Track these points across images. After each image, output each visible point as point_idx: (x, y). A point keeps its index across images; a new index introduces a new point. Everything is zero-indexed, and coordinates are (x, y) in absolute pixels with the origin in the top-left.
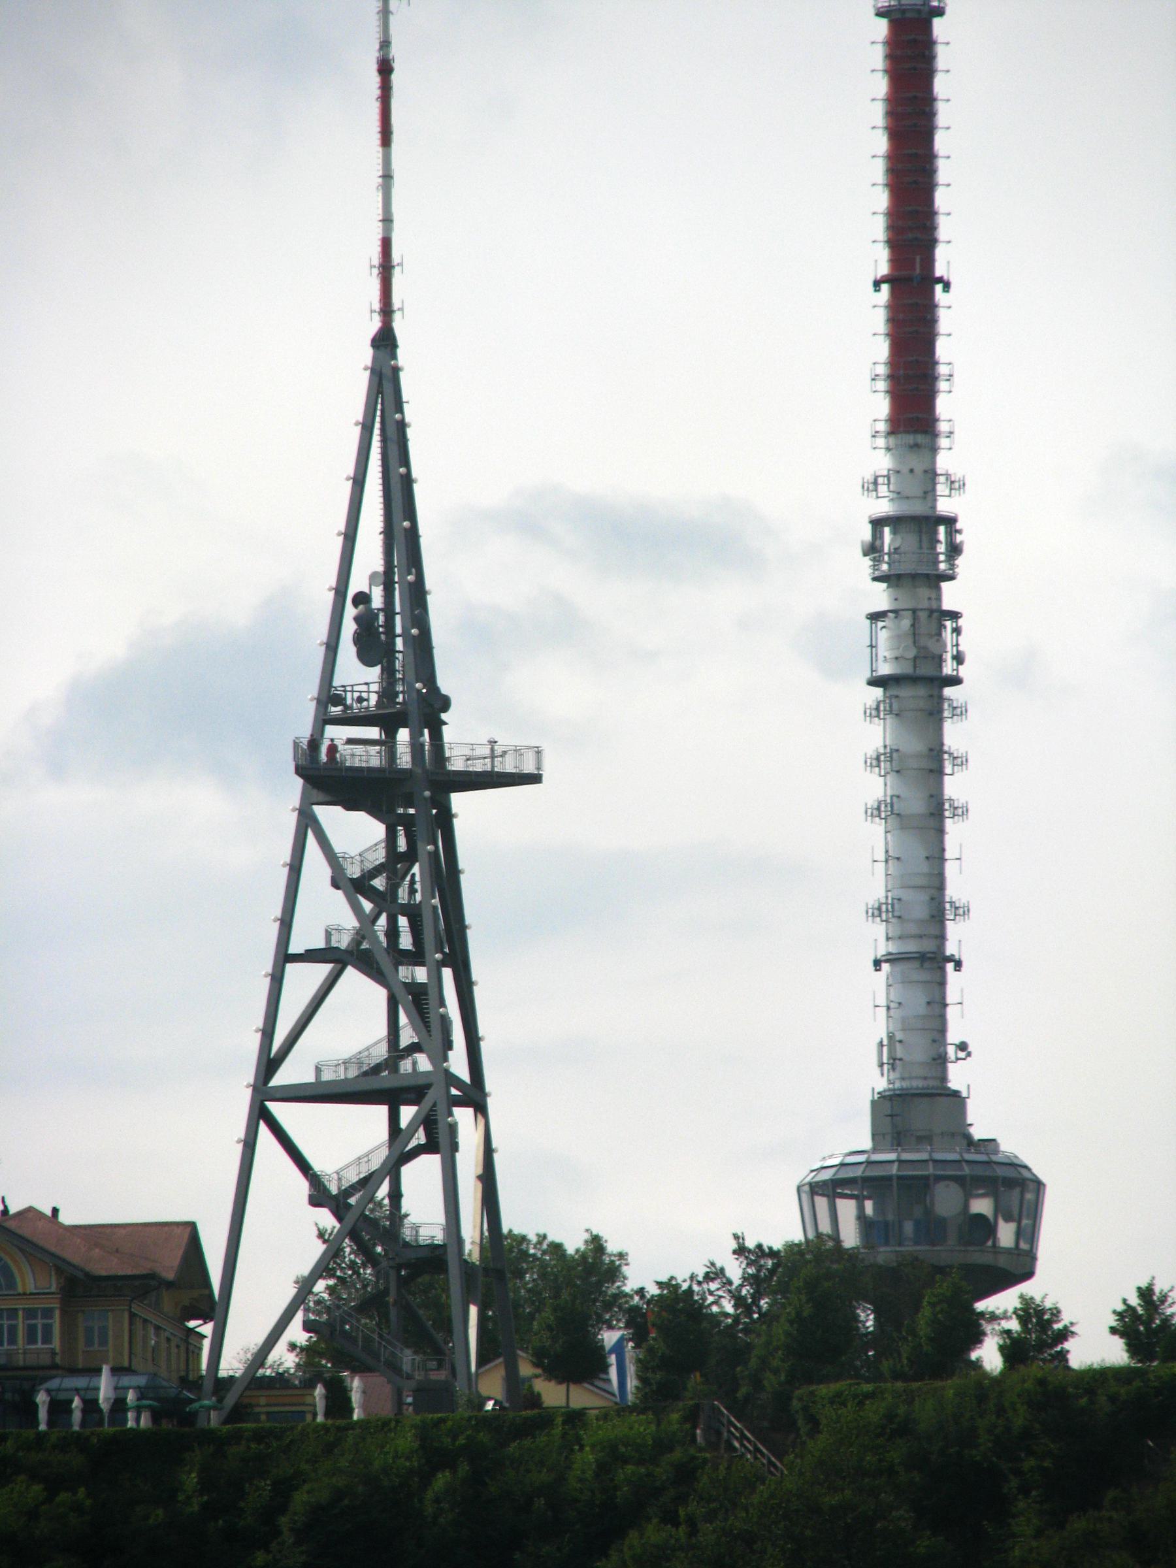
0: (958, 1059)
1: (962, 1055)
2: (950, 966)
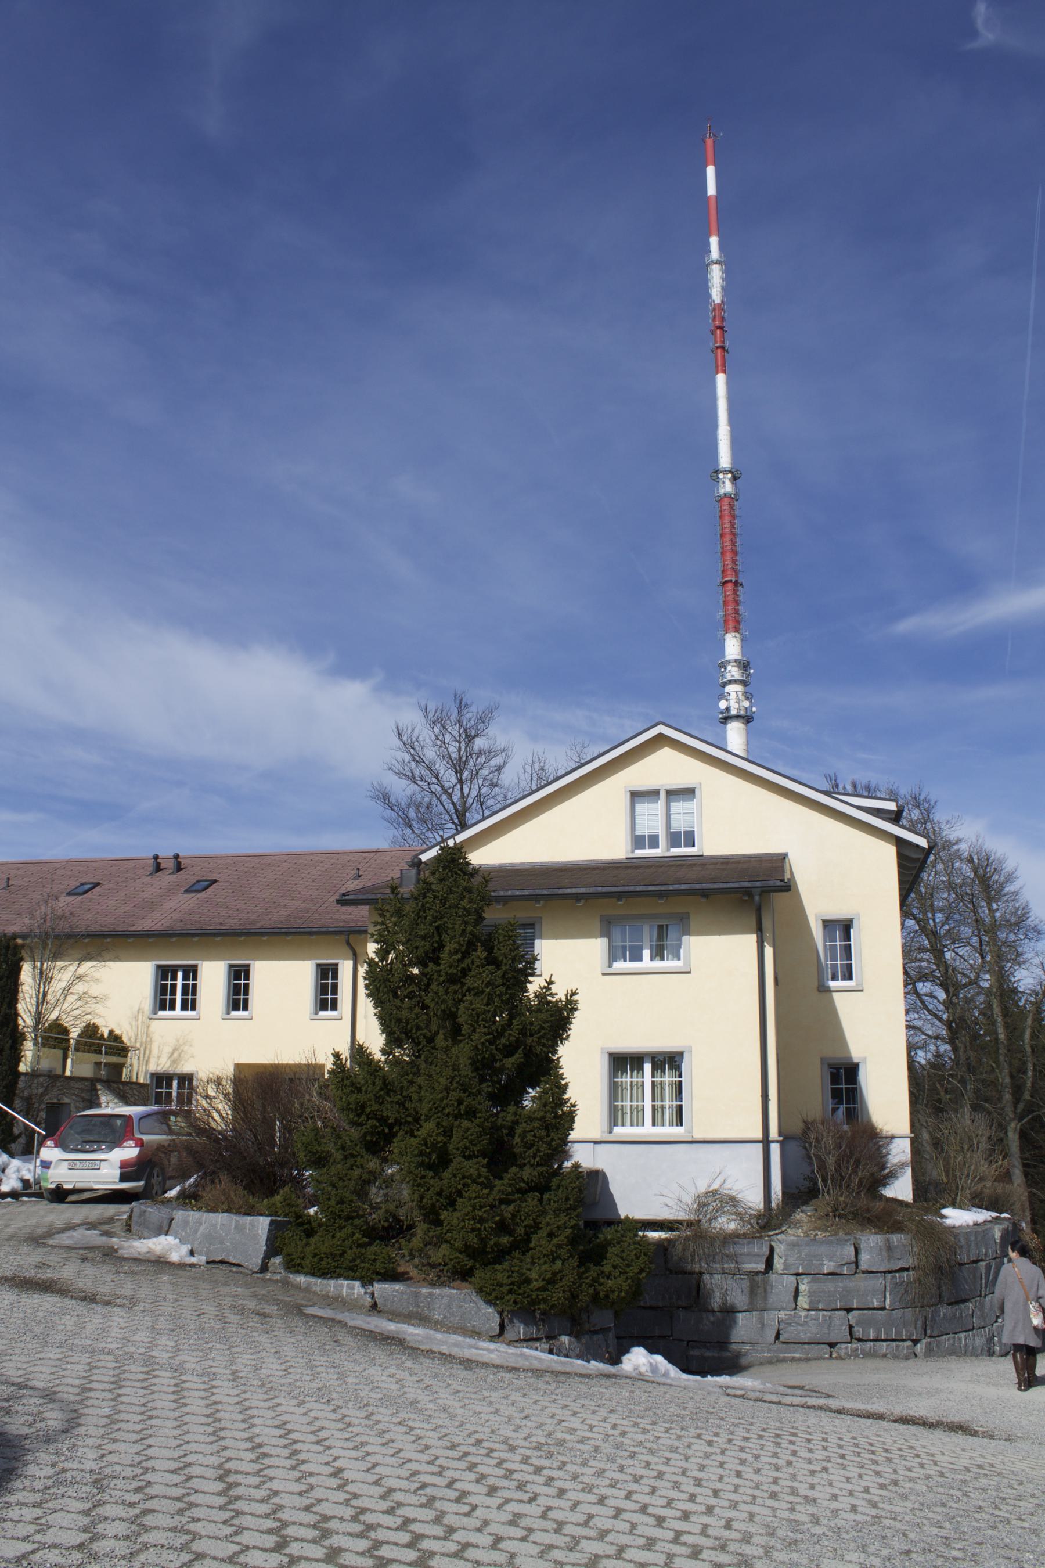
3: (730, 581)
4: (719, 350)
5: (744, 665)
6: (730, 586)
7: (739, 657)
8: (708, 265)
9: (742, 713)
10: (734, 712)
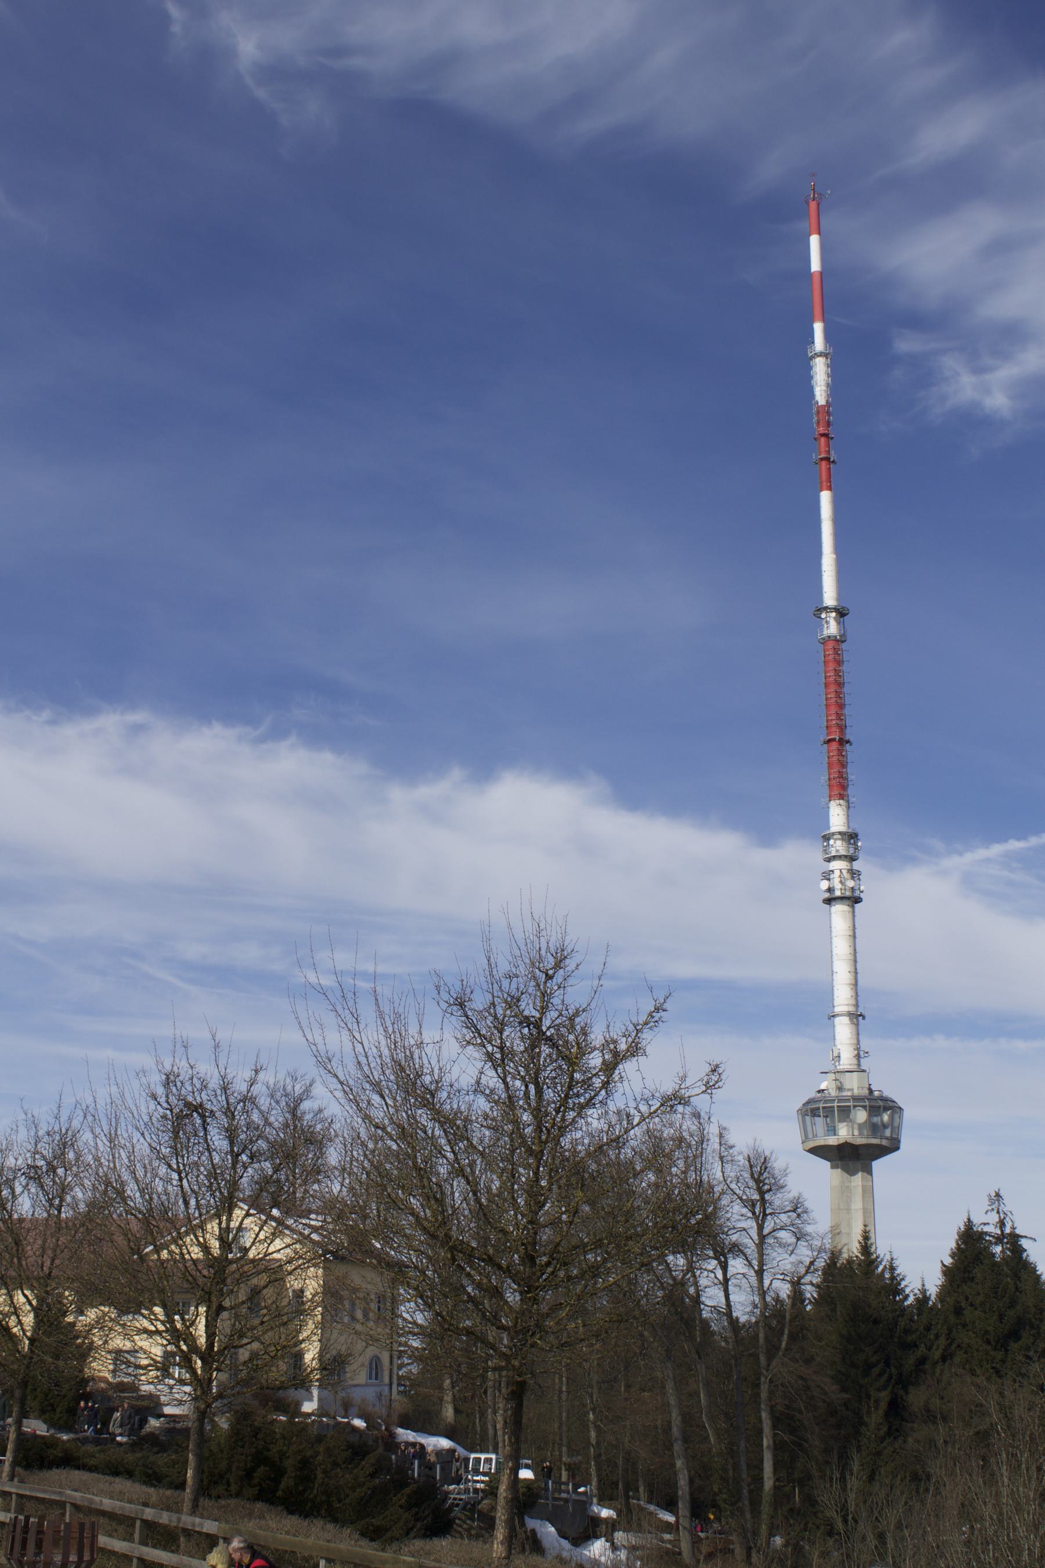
3: (834, 740)
4: (839, 912)
5: (851, 837)
6: (834, 746)
7: (843, 829)
8: (812, 358)
9: (848, 894)
10: (838, 893)
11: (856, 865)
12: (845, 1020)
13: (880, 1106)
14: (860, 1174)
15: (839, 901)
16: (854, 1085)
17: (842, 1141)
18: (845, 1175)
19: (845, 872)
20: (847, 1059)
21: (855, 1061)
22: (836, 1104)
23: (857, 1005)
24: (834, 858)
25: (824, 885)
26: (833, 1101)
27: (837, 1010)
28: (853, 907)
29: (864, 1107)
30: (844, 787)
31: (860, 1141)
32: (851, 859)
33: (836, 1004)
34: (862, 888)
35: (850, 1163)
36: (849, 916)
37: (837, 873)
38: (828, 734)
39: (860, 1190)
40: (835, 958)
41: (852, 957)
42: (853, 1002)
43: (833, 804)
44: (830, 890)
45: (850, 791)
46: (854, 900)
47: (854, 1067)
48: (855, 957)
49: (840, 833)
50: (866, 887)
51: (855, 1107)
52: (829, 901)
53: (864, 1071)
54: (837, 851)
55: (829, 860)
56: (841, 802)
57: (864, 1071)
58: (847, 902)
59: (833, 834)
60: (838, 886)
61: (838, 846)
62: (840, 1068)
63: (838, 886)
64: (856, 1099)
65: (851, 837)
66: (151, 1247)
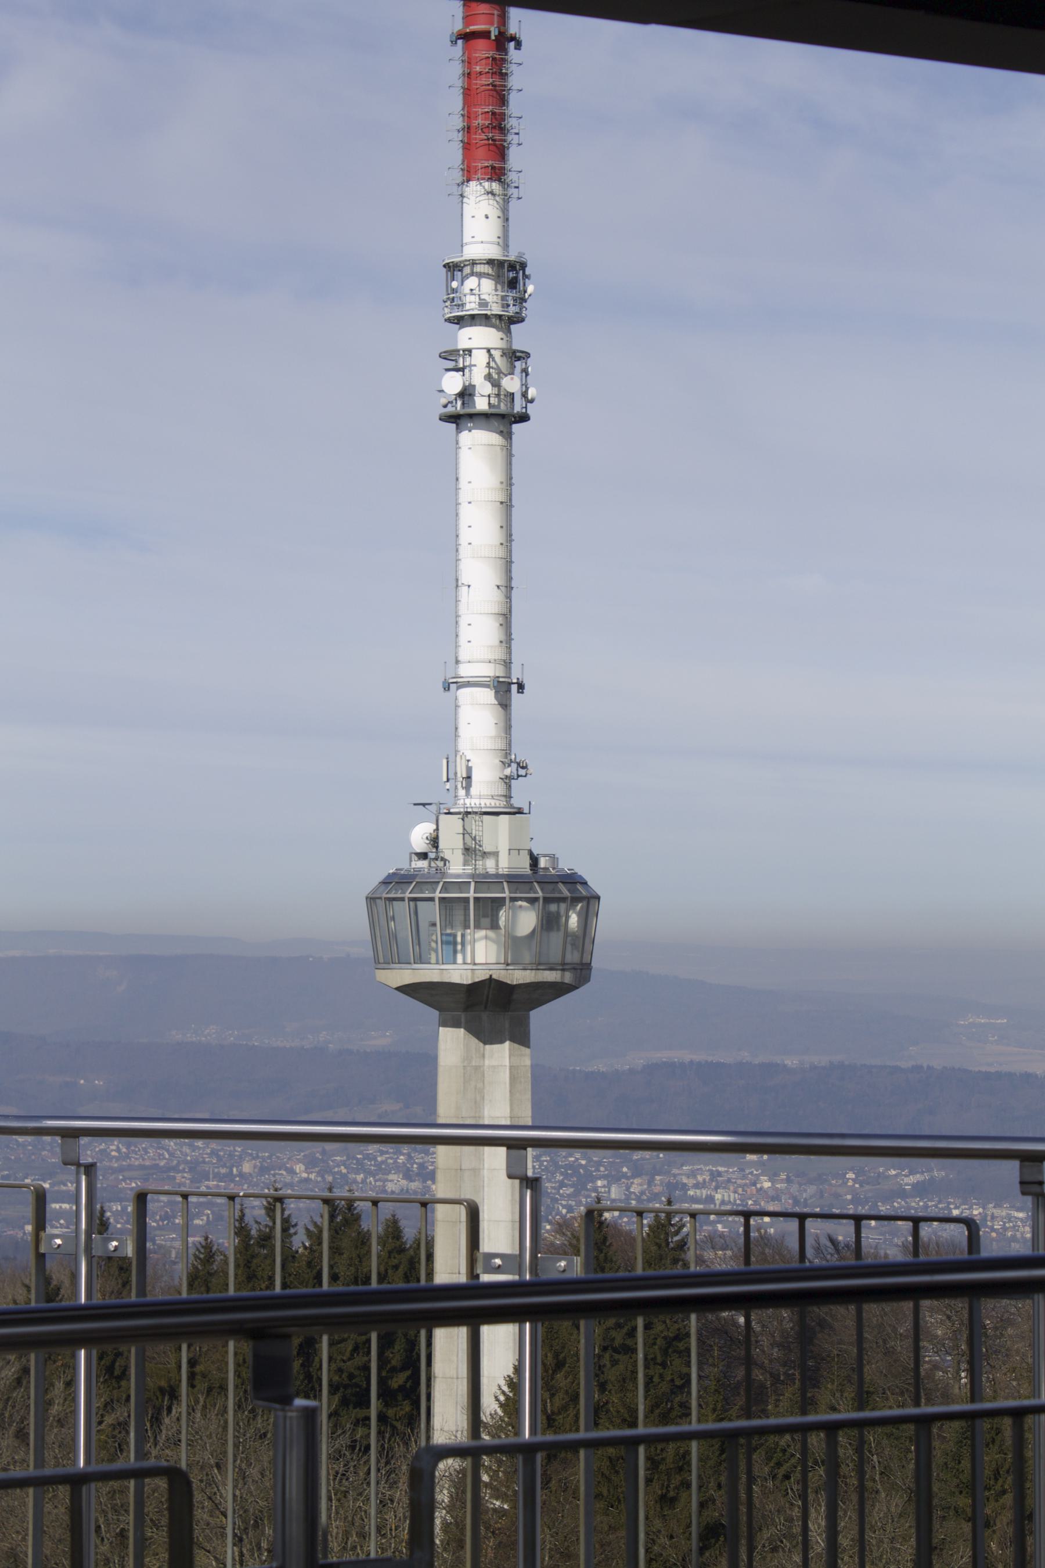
0: (518, 776)
1: (522, 772)
2: (514, 688)
3: (486, 35)
4: (477, 447)
5: (510, 273)
6: (483, 50)
7: (494, 252)
9: (503, 408)
10: (481, 404)
11: (521, 337)
12: (487, 696)
13: (558, 891)
14: (507, 1043)
15: (482, 421)
16: (503, 848)
17: (481, 976)
18: (474, 1041)
19: (497, 354)
20: (485, 789)
21: (501, 789)
22: (471, 894)
23: (507, 664)
24: (473, 320)
25: (453, 383)
26: (463, 886)
27: (466, 671)
28: (508, 435)
29: (532, 901)
30: (500, 151)
31: (519, 976)
32: (507, 322)
33: (463, 656)
34: (532, 393)
35: (485, 1016)
36: (500, 456)
37: (480, 359)
38: (467, 19)
39: (505, 1076)
40: (464, 552)
41: (500, 552)
42: (499, 654)
43: (474, 189)
44: (466, 394)
45: (515, 158)
46: (506, 419)
47: (498, 804)
48: (510, 552)
49: (490, 262)
50: (542, 388)
51: (513, 900)
52: (459, 419)
53: (520, 812)
54: (483, 304)
55: (460, 321)
56: (495, 186)
57: (520, 812)
58: (495, 423)
59: (474, 263)
60: (484, 389)
61: (481, 292)
62: (472, 803)
63: (484, 389)
64: (514, 880)
65: (510, 273)
66: (854, 1176)
